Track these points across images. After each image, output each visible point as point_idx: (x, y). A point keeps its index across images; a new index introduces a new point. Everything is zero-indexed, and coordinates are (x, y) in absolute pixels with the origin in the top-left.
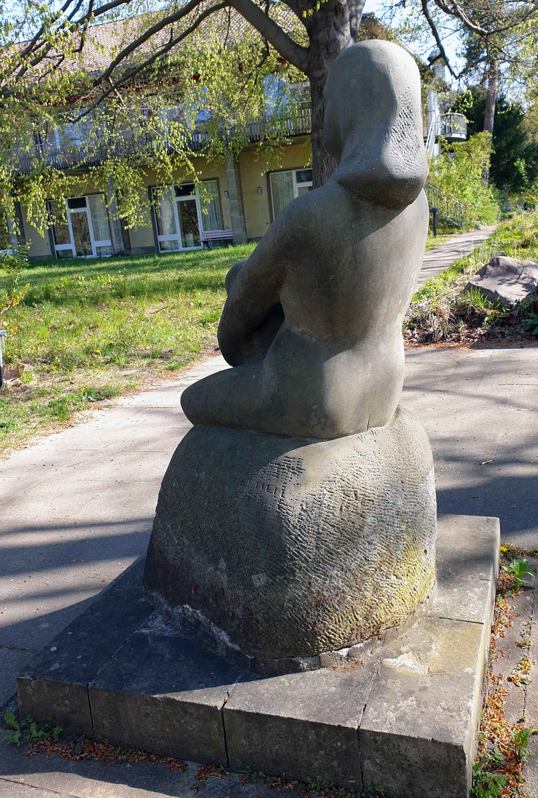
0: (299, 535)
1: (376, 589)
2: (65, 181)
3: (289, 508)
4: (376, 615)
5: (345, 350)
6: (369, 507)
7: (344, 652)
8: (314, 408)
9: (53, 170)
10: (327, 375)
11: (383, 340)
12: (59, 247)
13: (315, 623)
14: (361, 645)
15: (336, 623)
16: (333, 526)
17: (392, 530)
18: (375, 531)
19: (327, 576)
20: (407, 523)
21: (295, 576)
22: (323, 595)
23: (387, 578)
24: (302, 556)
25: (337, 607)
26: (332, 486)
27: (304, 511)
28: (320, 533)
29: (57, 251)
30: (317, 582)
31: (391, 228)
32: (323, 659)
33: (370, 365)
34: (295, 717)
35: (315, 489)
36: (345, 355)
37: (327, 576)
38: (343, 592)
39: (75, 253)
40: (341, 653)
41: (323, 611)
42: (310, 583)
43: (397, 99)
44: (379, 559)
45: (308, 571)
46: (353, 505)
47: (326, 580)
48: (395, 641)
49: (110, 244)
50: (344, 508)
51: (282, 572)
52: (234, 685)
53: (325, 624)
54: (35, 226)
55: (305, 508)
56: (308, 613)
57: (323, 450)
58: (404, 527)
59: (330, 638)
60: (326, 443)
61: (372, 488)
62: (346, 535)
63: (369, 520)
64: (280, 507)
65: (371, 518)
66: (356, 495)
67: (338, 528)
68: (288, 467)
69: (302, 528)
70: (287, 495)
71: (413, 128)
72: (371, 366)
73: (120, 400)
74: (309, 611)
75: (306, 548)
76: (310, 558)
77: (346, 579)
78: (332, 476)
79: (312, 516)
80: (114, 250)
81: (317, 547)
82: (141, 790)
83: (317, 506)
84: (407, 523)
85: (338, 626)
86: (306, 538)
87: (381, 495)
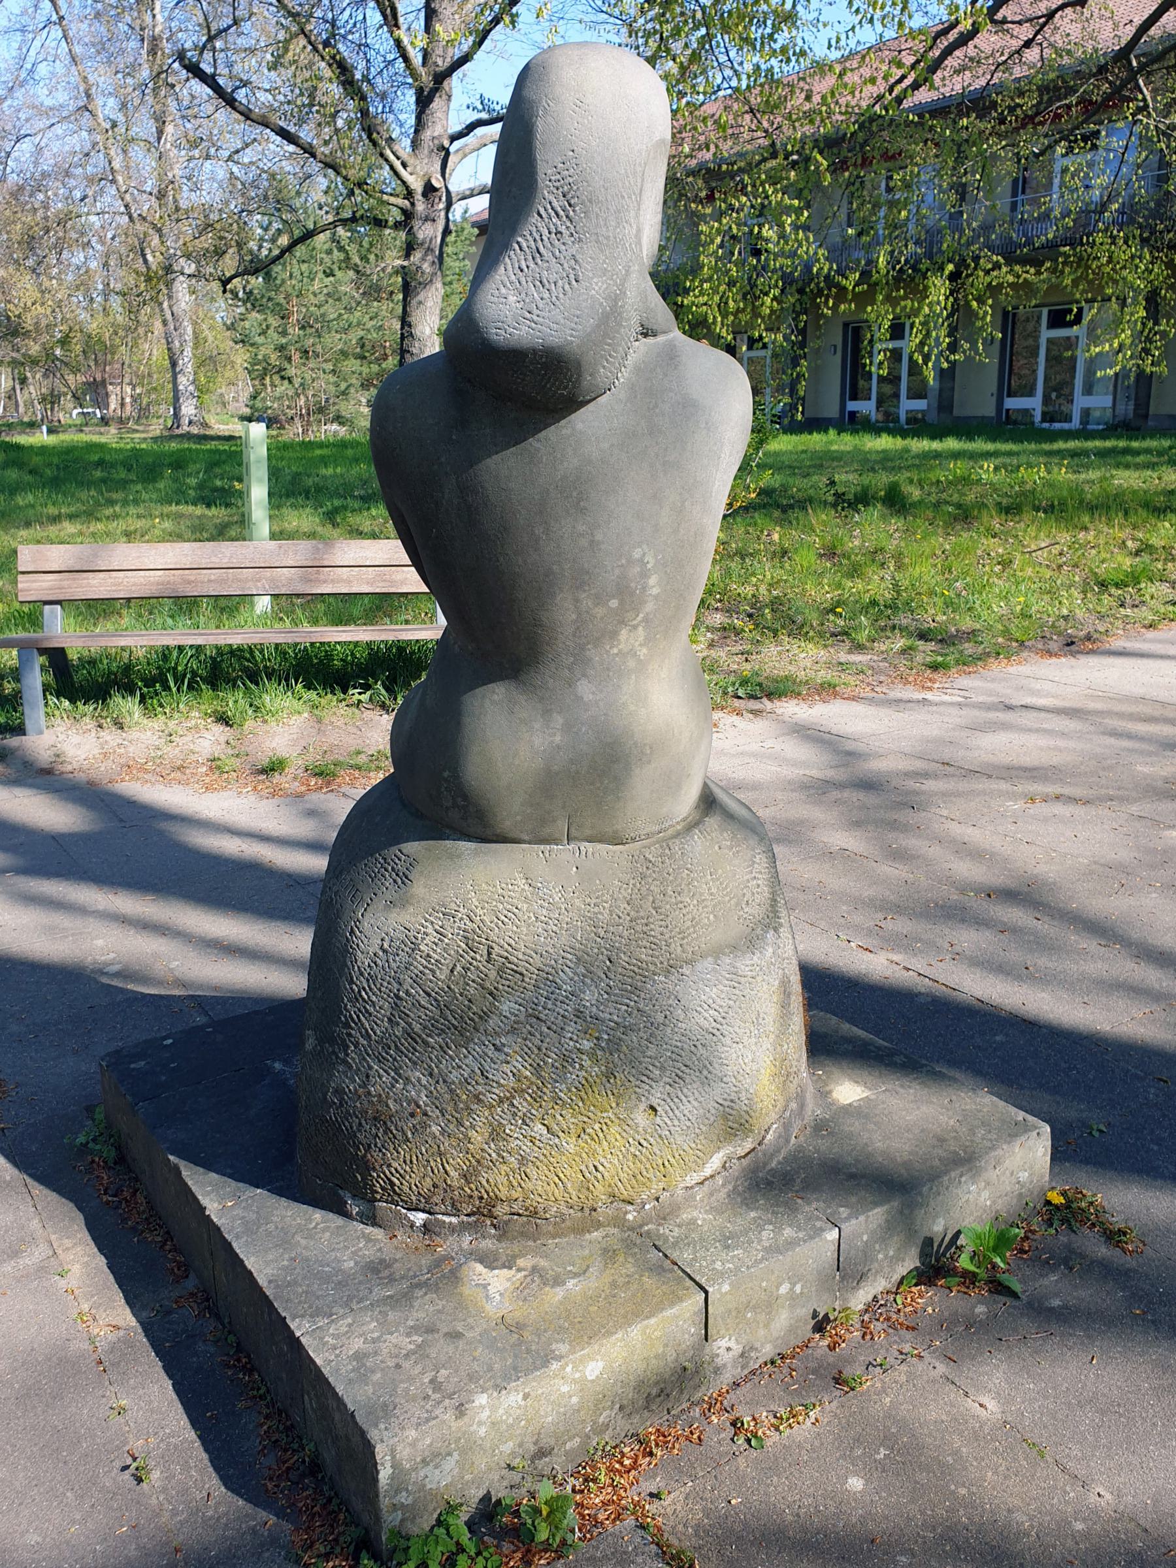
0: (364, 989)
1: (496, 1134)
2: (1005, 275)
3: (363, 938)
4: (488, 1181)
5: (503, 679)
6: (512, 984)
7: (419, 1218)
8: (446, 774)
9: (982, 254)
10: (466, 720)
11: (584, 675)
12: (1012, 403)
13: (369, 1146)
14: (454, 1220)
15: (405, 1162)
16: (429, 995)
17: (556, 1041)
18: (513, 1031)
19: (400, 1076)
20: (598, 1039)
21: (347, 1055)
22: (387, 1106)
23: (524, 1123)
24: (362, 1025)
25: (410, 1135)
26: (447, 924)
27: (385, 951)
28: (400, 999)
29: (1008, 410)
30: (381, 1081)
31: (538, 450)
32: (379, 1214)
33: (558, 720)
34: (255, 1275)
35: (413, 920)
36: (503, 690)
37: (400, 1076)
38: (425, 1114)
39: (1038, 418)
40: (412, 1218)
41: (385, 1133)
42: (368, 1076)
43: (541, 176)
44: (512, 1083)
45: (368, 1055)
46: (477, 968)
47: (397, 1082)
48: (530, 1243)
49: (1110, 405)
50: (459, 968)
51: (332, 1040)
52: (259, 1191)
53: (384, 1154)
54: (920, 361)
55: (386, 946)
56: (360, 1124)
57: (459, 856)
58: (587, 1045)
59: (392, 1184)
60: (471, 845)
61: (528, 951)
62: (450, 1018)
63: (507, 1006)
64: (352, 932)
65: (512, 1005)
66: (489, 953)
67: (436, 1000)
68: (393, 869)
69: (372, 978)
70: (368, 915)
71: (569, 240)
72: (561, 721)
73: (790, 709)
74: (363, 1122)
75: (370, 1015)
76: (375, 1033)
77: (435, 1092)
78: (453, 906)
79: (393, 965)
80: (1114, 416)
81: (389, 1019)
82: (111, 1277)
83: (407, 949)
84: (598, 1039)
85: (408, 1169)
86: (374, 998)
87: (547, 969)
